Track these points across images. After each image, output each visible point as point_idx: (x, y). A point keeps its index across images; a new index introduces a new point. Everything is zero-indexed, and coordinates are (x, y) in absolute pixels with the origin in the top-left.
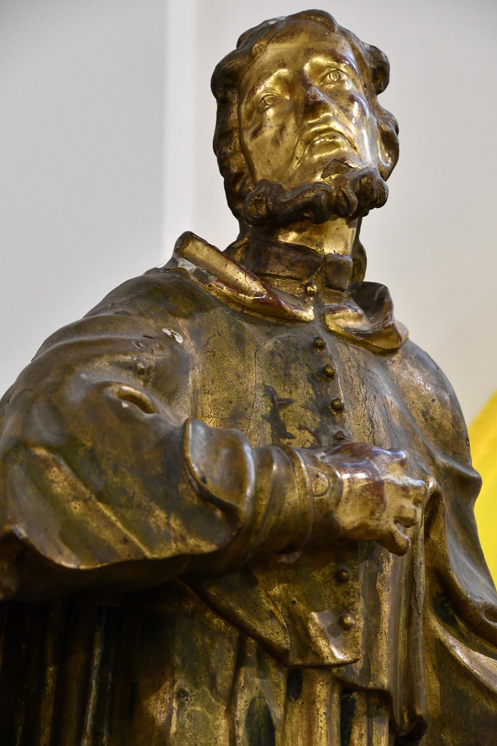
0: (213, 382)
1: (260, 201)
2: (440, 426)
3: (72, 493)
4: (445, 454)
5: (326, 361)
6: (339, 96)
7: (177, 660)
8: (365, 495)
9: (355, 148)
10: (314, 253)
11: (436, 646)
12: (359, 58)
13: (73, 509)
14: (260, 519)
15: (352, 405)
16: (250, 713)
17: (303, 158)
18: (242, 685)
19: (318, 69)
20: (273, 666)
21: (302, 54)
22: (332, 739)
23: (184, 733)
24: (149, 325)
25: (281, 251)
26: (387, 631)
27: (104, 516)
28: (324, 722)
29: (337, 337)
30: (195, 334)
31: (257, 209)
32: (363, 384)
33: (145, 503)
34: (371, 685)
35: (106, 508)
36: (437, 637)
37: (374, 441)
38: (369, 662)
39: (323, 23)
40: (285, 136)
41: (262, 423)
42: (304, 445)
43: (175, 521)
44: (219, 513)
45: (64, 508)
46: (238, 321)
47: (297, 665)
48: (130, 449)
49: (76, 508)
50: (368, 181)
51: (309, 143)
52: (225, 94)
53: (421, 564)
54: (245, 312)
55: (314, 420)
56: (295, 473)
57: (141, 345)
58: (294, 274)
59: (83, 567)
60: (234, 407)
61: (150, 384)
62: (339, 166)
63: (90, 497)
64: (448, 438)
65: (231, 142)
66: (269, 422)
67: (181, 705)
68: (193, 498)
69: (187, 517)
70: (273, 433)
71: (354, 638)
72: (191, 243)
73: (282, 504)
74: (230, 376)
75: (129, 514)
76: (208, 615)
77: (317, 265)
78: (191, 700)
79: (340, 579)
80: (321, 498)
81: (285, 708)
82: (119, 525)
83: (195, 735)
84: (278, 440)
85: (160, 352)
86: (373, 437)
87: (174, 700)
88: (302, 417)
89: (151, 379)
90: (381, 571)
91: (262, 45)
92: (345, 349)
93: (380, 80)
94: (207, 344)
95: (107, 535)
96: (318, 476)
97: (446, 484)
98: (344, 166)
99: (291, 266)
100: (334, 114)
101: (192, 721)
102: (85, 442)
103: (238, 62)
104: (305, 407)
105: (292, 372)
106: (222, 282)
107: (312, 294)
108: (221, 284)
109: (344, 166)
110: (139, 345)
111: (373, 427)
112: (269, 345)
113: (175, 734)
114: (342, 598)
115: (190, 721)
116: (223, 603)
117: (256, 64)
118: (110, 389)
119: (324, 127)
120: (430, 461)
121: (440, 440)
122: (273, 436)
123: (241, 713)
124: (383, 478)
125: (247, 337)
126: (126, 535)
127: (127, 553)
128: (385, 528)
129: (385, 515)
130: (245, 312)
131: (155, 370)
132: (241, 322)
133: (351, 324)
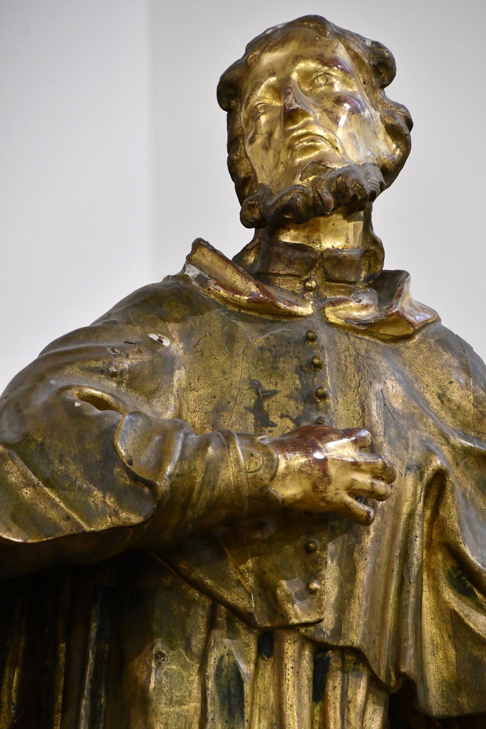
0: (199, 379)
1: (253, 205)
2: (459, 408)
3: (24, 481)
4: (466, 437)
5: (317, 352)
6: (325, 99)
7: (156, 628)
8: (305, 470)
9: (337, 148)
10: (312, 250)
11: (451, 615)
12: (355, 57)
13: (24, 494)
14: (195, 494)
15: (342, 391)
16: (219, 669)
17: (287, 163)
18: (212, 645)
19: (307, 76)
20: (243, 628)
21: (291, 61)
22: (300, 690)
23: (161, 688)
24: (135, 333)
25: (281, 250)
26: (360, 596)
27: (50, 499)
28: (291, 675)
29: (337, 328)
30: (186, 336)
31: (251, 213)
32: (359, 371)
33: (85, 486)
34: (341, 643)
35: (51, 491)
36: (452, 608)
37: (364, 425)
38: (340, 621)
39: (315, 28)
40: (272, 142)
41: (245, 414)
42: (284, 432)
43: (109, 499)
44: (147, 490)
45: (17, 494)
46: (233, 321)
47: (267, 627)
48: (74, 441)
49: (27, 493)
50: (342, 180)
51: (291, 147)
52: (229, 103)
53: (417, 537)
54: (242, 311)
55: (297, 408)
56: (229, 453)
57: (116, 350)
58: (293, 272)
59: (29, 541)
60: (218, 401)
61: (124, 385)
62: (317, 168)
63: (38, 483)
64: (470, 418)
65: (238, 148)
66: (253, 413)
67: (159, 665)
68: (126, 479)
69: (121, 495)
70: (256, 422)
71: (320, 601)
72: (198, 250)
73: (216, 482)
74: (216, 373)
75: (71, 496)
76: (184, 587)
77: (315, 261)
78: (168, 660)
79: (309, 551)
80: (254, 474)
81: (257, 665)
82: (62, 504)
83: (171, 689)
84: (261, 429)
85: (138, 356)
86: (363, 420)
87: (153, 661)
88: (284, 406)
89: (125, 381)
90: (360, 542)
91: (256, 55)
92: (344, 339)
93: (383, 75)
94: (197, 344)
95: (53, 514)
96: (252, 455)
97: (466, 463)
98: (322, 167)
99: (290, 263)
100: (315, 118)
101: (169, 678)
102: (36, 437)
103: (237, 73)
104: (290, 397)
105: (281, 365)
106: (219, 285)
107: (311, 289)
108: (218, 287)
109: (322, 167)
110: (114, 351)
111: (363, 411)
112: (260, 341)
113: (154, 689)
114: (310, 567)
115: (167, 678)
116: (193, 575)
117: (252, 73)
118: (69, 392)
119: (304, 131)
120: (443, 441)
121: (460, 421)
122: (256, 426)
123: (211, 670)
124: (326, 454)
125: (239, 335)
126: (68, 513)
127: (70, 528)
128: (337, 499)
129: (331, 488)
130: (242, 311)
131: (129, 372)
132: (235, 321)
133: (355, 314)
